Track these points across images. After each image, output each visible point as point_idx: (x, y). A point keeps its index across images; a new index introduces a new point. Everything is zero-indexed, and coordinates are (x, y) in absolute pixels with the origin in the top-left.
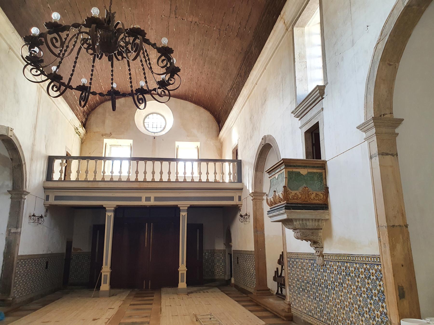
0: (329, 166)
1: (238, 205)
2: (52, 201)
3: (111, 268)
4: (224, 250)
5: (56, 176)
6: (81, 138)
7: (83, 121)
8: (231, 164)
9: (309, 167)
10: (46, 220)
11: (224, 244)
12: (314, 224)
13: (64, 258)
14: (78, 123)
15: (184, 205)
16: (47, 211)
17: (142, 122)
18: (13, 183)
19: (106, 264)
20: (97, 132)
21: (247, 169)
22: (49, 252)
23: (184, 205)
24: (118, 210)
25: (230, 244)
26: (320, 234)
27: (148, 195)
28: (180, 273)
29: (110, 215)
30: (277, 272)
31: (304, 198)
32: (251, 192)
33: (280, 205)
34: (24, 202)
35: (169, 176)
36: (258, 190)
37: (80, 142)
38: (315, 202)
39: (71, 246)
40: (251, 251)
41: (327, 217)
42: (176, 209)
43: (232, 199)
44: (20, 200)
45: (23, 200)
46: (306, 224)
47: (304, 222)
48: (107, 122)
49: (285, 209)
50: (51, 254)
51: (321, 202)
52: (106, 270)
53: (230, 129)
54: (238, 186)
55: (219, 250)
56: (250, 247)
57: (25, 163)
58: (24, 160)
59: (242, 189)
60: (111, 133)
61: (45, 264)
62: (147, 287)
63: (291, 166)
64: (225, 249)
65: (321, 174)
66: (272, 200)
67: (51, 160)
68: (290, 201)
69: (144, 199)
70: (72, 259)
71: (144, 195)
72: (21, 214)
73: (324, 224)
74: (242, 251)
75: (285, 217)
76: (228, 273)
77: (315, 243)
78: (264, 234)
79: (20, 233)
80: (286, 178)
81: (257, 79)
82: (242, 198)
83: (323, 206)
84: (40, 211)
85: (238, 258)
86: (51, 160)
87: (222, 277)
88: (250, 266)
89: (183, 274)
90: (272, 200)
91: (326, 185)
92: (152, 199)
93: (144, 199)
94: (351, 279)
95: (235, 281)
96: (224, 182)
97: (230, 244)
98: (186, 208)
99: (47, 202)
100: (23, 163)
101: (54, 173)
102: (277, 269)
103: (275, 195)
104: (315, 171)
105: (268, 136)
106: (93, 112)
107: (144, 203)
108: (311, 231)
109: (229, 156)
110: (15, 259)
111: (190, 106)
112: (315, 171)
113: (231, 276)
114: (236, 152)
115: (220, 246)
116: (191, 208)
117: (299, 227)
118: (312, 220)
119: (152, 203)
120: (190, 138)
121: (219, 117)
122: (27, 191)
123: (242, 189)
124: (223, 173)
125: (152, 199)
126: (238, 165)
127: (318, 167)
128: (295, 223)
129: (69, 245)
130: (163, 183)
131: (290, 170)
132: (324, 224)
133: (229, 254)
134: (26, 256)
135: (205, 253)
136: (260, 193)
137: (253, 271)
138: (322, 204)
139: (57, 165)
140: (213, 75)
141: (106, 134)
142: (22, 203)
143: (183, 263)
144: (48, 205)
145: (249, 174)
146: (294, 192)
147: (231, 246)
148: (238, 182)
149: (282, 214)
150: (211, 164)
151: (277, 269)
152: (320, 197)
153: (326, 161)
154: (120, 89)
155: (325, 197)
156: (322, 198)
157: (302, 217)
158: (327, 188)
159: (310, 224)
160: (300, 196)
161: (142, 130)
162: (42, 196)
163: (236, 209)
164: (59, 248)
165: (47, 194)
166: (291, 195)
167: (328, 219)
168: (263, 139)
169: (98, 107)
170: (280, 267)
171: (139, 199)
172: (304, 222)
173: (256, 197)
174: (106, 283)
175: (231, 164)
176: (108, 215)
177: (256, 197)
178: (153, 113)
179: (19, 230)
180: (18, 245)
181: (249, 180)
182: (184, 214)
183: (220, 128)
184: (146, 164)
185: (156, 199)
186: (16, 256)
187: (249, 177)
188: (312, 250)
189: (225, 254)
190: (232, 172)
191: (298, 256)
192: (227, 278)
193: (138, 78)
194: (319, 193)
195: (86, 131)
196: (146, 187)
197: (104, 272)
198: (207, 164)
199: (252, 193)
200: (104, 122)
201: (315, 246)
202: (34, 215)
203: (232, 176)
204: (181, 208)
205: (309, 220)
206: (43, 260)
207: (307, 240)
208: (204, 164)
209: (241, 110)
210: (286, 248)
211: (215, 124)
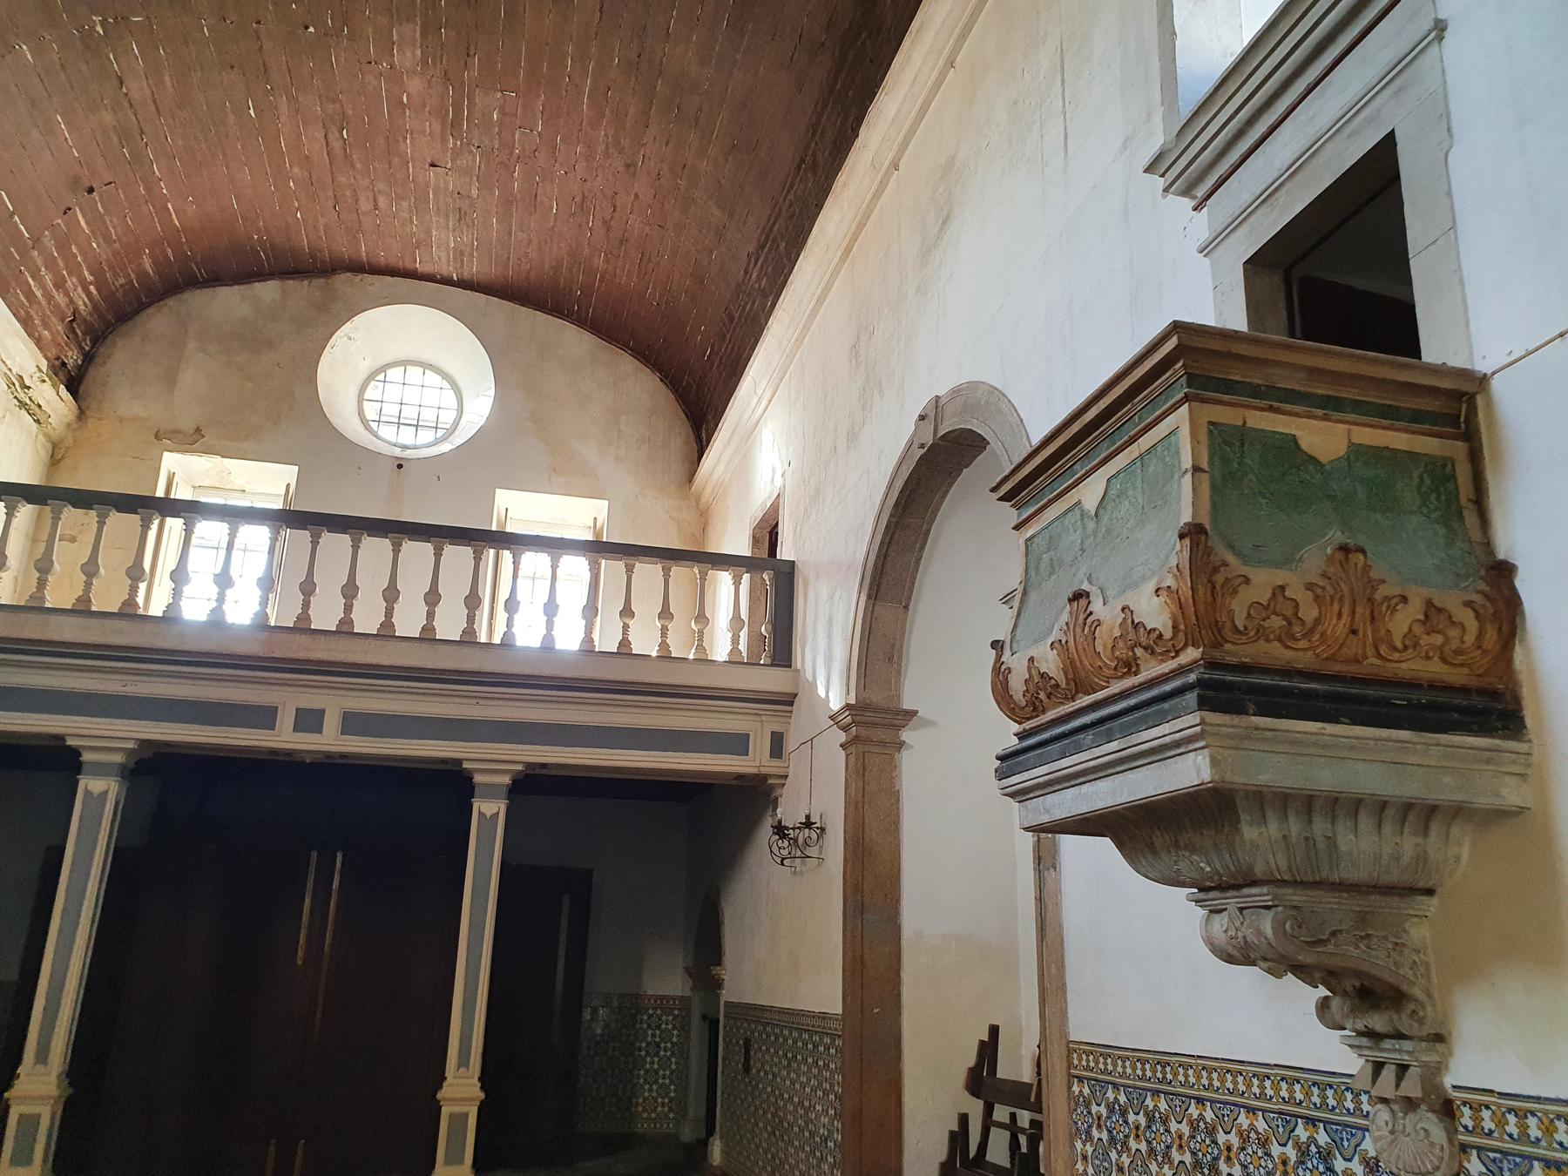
0: (1515, 406)
1: (765, 777)
4: (682, 998)
6: (47, 436)
7: (70, 362)
8: (746, 577)
9: (1358, 407)
11: (686, 969)
12: (1387, 850)
14: (26, 358)
15: (493, 763)
19: (42, 1056)
20: (134, 419)
21: (824, 592)
23: (493, 763)
24: (152, 768)
25: (715, 970)
26: (1418, 933)
28: (445, 1111)
29: (99, 790)
30: (958, 1138)
31: (1342, 628)
32: (835, 704)
33: (1123, 695)
35: (431, 615)
36: (876, 697)
37: (44, 455)
38: (1411, 667)
40: (823, 1016)
41: (1512, 794)
42: (453, 784)
46: (1331, 841)
47: (1320, 827)
48: (189, 377)
49: (1203, 704)
51: (1458, 677)
53: (749, 436)
54: (771, 680)
55: (662, 998)
56: (821, 990)
59: (787, 700)
63: (1229, 387)
64: (688, 993)
65: (1439, 473)
66: (1050, 663)
68: (1236, 652)
69: (286, 720)
71: (289, 700)
73: (1465, 852)
74: (771, 1009)
75: (1191, 771)
76: (696, 1108)
77: (1369, 999)
78: (897, 929)
80: (1196, 469)
81: (900, 139)
82: (790, 744)
83: (1477, 702)
85: (747, 1044)
87: (667, 1127)
88: (815, 1100)
89: (459, 1120)
90: (1050, 663)
91: (1488, 546)
92: (331, 723)
93: (286, 720)
95: (726, 1153)
96: (703, 661)
97: (715, 970)
98: (506, 780)
102: (964, 1119)
103: (1086, 623)
104: (1400, 440)
105: (956, 392)
107: (284, 737)
108: (1353, 904)
109: (738, 543)
111: (575, 341)
112: (1400, 440)
113: (710, 1132)
114: (768, 533)
115: (667, 980)
116: (531, 786)
117: (1279, 863)
118: (1382, 806)
119: (330, 740)
120: (563, 475)
121: (698, 397)
123: (787, 700)
124: (702, 618)
125: (331, 723)
126: (774, 575)
127: (1417, 417)
128: (1249, 832)
130: (391, 645)
131: (1229, 416)
132: (1465, 852)
133: (704, 1017)
135: (595, 1011)
136: (887, 711)
137: (826, 1121)
138: (1464, 690)
140: (682, 183)
143: (463, 1061)
145: (830, 621)
146: (1263, 580)
147: (718, 984)
148: (772, 665)
149: (1177, 747)
150: (648, 572)
151: (964, 1119)
152: (1454, 633)
153: (1483, 380)
154: (258, 232)
155: (1491, 633)
156: (1470, 638)
157: (1325, 777)
158: (1503, 572)
159: (1363, 848)
160: (1309, 613)
161: (350, 427)
163: (752, 797)
166: (1248, 595)
167: (1521, 811)
168: (922, 418)
169: (151, 310)
170: (975, 1108)
171: (265, 717)
172: (1320, 827)
173: (864, 732)
174: (28, 1161)
175: (746, 577)
176: (87, 793)
177: (864, 732)
178: (405, 363)
181: (830, 649)
182: (489, 809)
183: (701, 444)
184: (315, 543)
185: (353, 723)
187: (829, 637)
188: (1333, 1052)
189: (684, 1028)
190: (744, 615)
191: (1159, 1076)
192: (687, 1134)
193: (342, 179)
194: (1452, 601)
196: (302, 655)
197: (24, 1099)
198: (630, 570)
199: (848, 707)
201: (1378, 1022)
203: (744, 634)
204: (478, 778)
205: (1356, 805)
207: (1303, 972)
208: (612, 569)
209: (806, 328)
210: (1063, 1014)
211: (680, 432)
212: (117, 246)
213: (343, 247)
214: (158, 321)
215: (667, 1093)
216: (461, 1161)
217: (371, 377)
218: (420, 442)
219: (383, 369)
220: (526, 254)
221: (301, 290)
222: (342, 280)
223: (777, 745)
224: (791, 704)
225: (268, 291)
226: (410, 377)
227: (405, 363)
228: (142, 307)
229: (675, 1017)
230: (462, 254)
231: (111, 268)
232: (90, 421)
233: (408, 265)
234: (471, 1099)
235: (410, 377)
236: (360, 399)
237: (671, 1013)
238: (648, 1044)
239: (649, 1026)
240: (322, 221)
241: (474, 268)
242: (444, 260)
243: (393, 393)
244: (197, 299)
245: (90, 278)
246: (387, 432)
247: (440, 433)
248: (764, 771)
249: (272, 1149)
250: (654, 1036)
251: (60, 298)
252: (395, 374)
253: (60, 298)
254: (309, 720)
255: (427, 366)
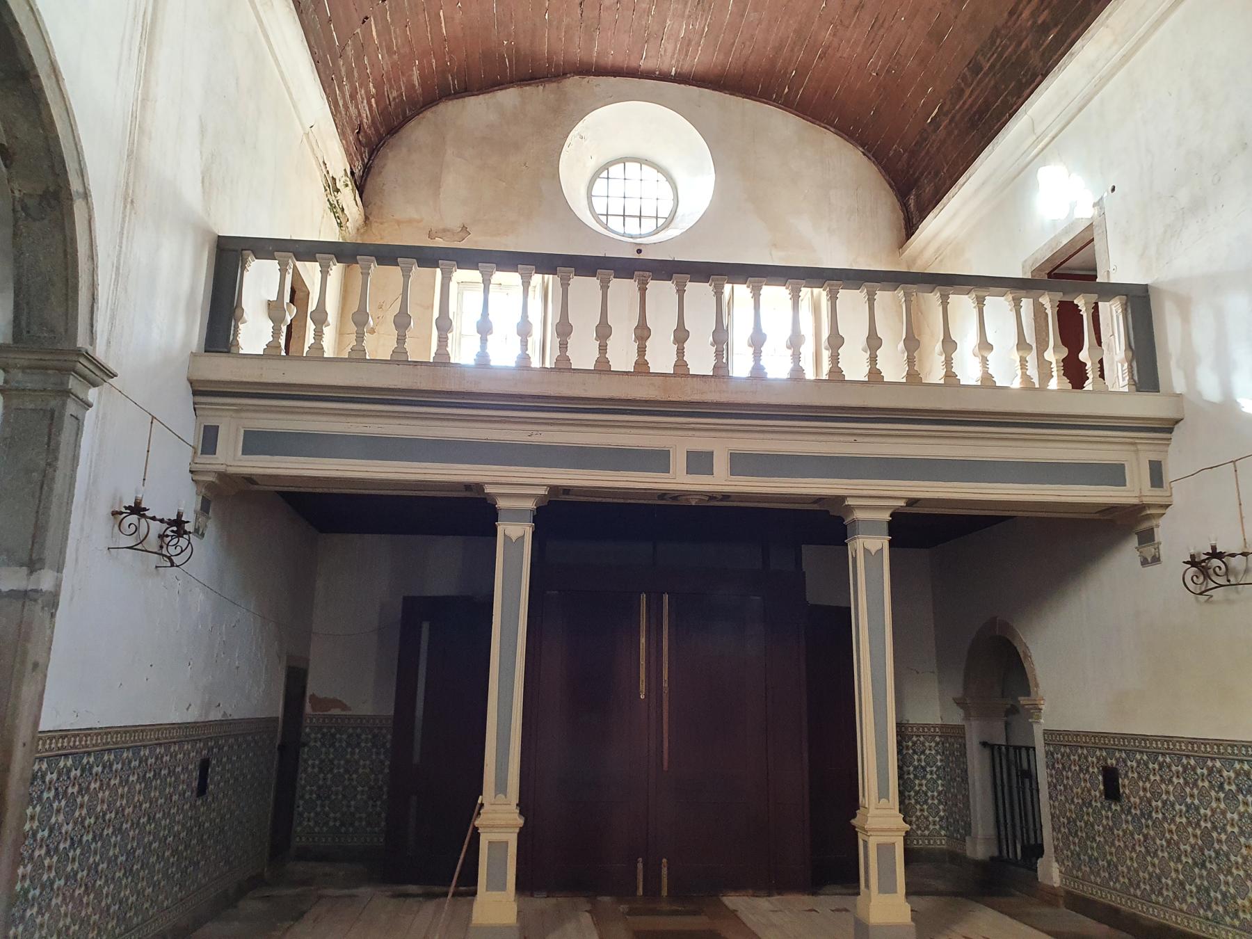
2: (231, 457)
3: (523, 807)
5: (254, 334)
10: (202, 553)
13: (278, 742)
14: (339, 164)
16: (205, 507)
17: (583, 192)
18: (17, 306)
19: (501, 787)
22: (215, 715)
27: (700, 443)
28: (873, 842)
29: (516, 535)
34: (78, 422)
39: (304, 688)
42: (826, 525)
43: (1114, 475)
44: (53, 403)
45: (71, 408)
50: (220, 723)
52: (499, 818)
54: (1147, 406)
55: (924, 726)
57: (86, 195)
58: (82, 173)
59: (1166, 427)
60: (464, 228)
61: (196, 774)
62: (652, 890)
67: (229, 257)
69: (679, 462)
70: (305, 745)
72: (59, 486)
79: (52, 601)
82: (1170, 474)
84: (174, 495)
86: (229, 257)
89: (885, 850)
92: (721, 464)
93: (679, 462)
94: (1094, 812)
98: (886, 516)
99: (207, 459)
100: (75, 185)
101: (240, 318)
106: (392, 141)
107: (678, 479)
110: (19, 754)
111: (781, 124)
119: (721, 480)
122: (100, 353)
125: (721, 464)
129: (296, 680)
134: (87, 732)
139: (260, 282)
141: (444, 230)
142: (68, 424)
144: (210, 478)
162: (183, 418)
164: (253, 697)
165: (212, 422)
169: (412, 123)
171: (659, 460)
178: (624, 160)
179: (45, 581)
180: (40, 668)
185: (740, 463)
186: (23, 734)
195: (367, 218)
200: (435, 183)
202: (137, 509)
206: (187, 754)
212: (396, 57)
213: (578, 50)
214: (419, 132)
215: (938, 813)
216: (894, 890)
217: (596, 176)
218: (645, 231)
219: (606, 167)
220: (752, 36)
221: (537, 95)
222: (572, 84)
223: (1156, 474)
224: (1170, 430)
225: (509, 97)
226: (640, 167)
227: (624, 160)
228: (406, 120)
229: (937, 744)
230: (690, 41)
231: (389, 80)
232: (375, 225)
233: (633, 64)
234: (898, 830)
235: (640, 167)
236: (590, 196)
237: (933, 740)
238: (916, 768)
239: (915, 752)
240: (566, 20)
241: (697, 60)
242: (669, 54)
243: (616, 187)
244: (449, 109)
245: (373, 91)
246: (615, 224)
247: (661, 222)
248: (1146, 500)
249: (640, 866)
250: (919, 760)
251: (353, 110)
252: (616, 170)
253: (353, 110)
254: (700, 462)
255: (642, 161)
